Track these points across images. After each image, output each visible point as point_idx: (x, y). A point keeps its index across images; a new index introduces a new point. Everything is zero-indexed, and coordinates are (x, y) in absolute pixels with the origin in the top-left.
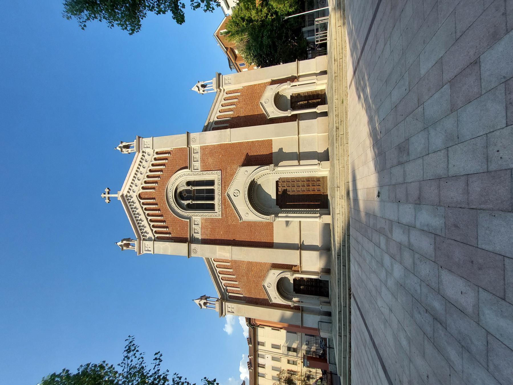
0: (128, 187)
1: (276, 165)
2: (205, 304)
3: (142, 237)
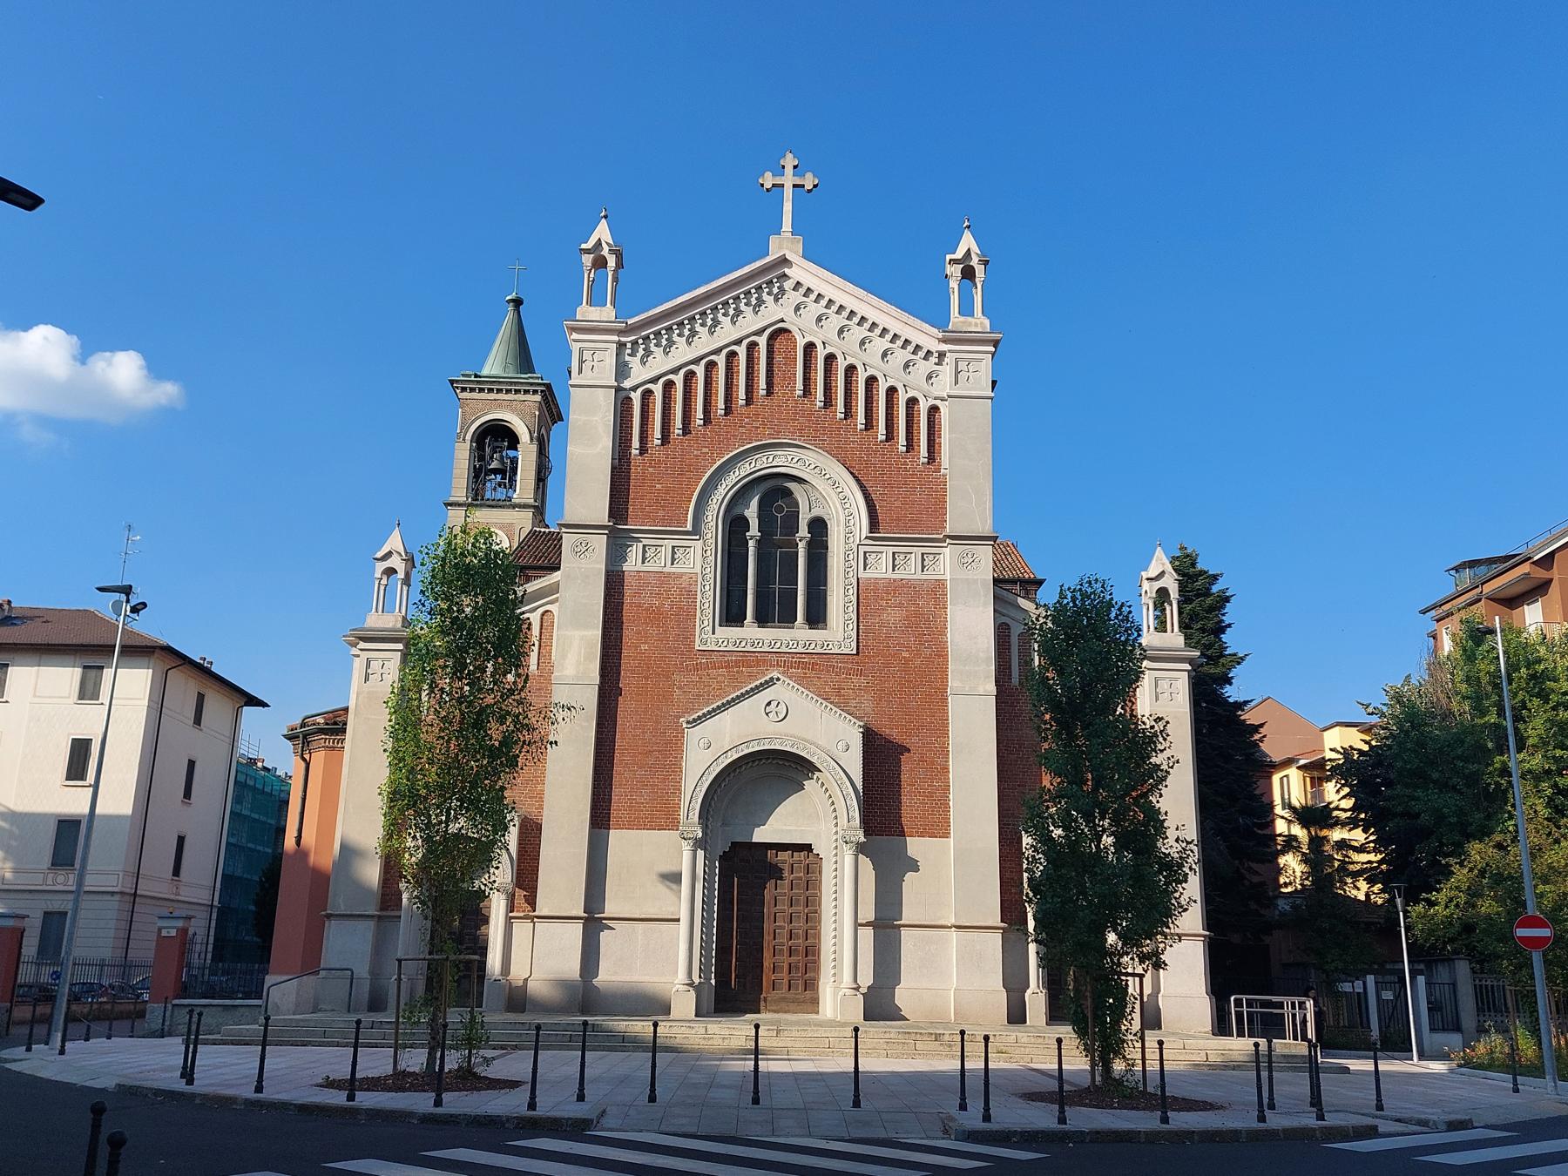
0: (818, 287)
1: (861, 849)
2: (390, 572)
3: (634, 337)
